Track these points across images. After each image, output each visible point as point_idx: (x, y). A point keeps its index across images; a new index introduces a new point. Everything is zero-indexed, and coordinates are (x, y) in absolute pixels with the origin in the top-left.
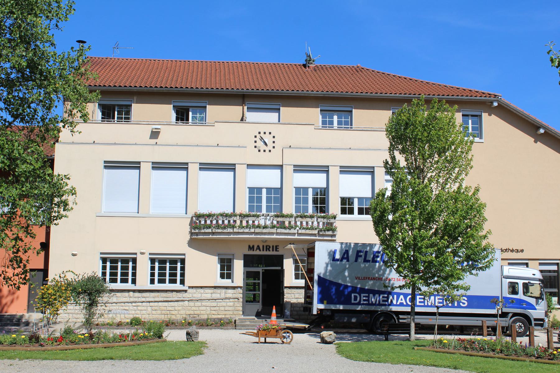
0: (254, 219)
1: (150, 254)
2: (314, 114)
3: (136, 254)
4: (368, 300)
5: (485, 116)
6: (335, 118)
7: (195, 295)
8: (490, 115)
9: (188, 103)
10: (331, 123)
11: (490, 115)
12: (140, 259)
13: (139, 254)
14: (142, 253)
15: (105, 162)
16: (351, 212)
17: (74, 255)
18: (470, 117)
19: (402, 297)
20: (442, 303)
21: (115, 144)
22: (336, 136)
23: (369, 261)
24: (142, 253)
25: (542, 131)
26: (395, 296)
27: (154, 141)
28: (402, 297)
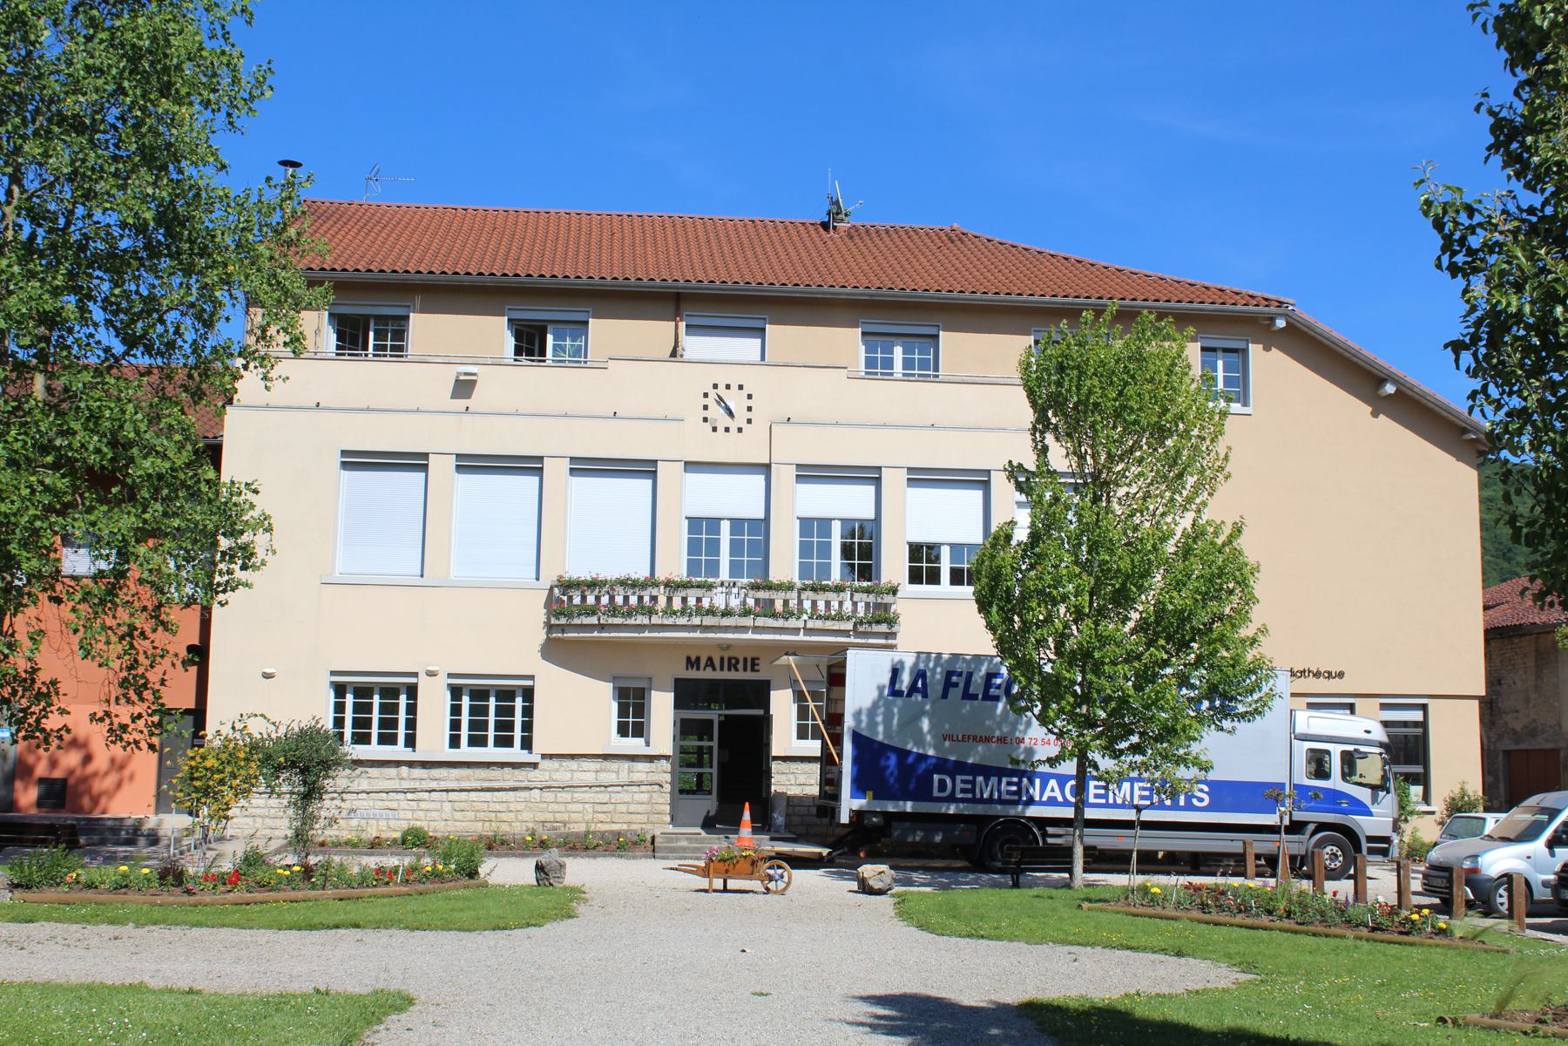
0: (699, 592)
1: (450, 676)
2: (847, 341)
3: (415, 675)
4: (973, 791)
5: (1255, 350)
6: (898, 352)
7: (557, 776)
8: (1267, 349)
9: (543, 312)
10: (888, 364)
11: (1267, 349)
12: (424, 686)
13: (422, 676)
14: (431, 674)
15: (344, 453)
16: (934, 578)
17: (267, 676)
18: (1220, 354)
19: (1053, 783)
20: (1149, 798)
21: (368, 409)
22: (900, 396)
23: (975, 697)
24: (431, 674)
25: (1390, 389)
26: (1037, 781)
27: (461, 404)
28: (1053, 783)
